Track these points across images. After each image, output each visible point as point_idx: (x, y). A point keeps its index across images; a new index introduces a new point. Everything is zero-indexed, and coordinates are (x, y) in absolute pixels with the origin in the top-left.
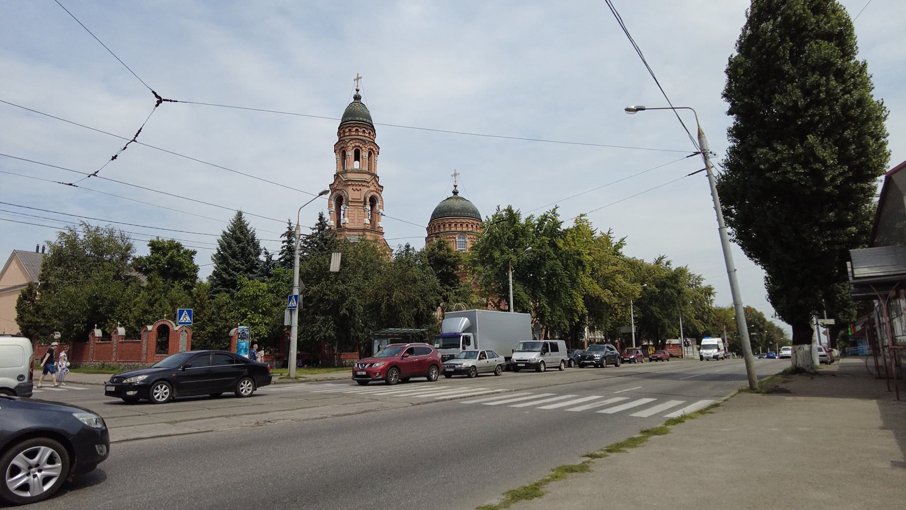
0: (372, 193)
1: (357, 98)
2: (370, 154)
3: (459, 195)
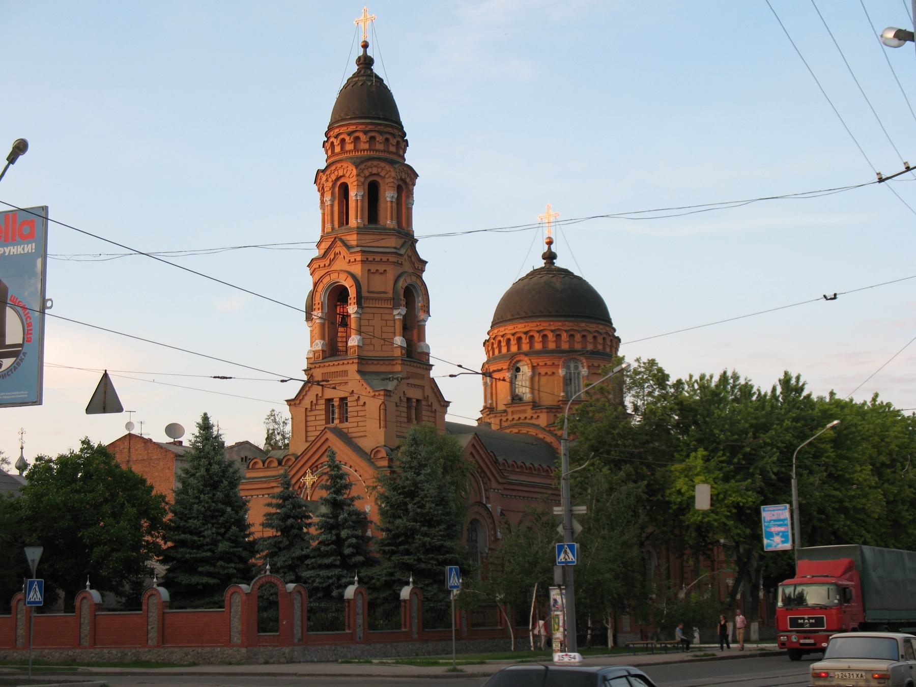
1: (366, 62)
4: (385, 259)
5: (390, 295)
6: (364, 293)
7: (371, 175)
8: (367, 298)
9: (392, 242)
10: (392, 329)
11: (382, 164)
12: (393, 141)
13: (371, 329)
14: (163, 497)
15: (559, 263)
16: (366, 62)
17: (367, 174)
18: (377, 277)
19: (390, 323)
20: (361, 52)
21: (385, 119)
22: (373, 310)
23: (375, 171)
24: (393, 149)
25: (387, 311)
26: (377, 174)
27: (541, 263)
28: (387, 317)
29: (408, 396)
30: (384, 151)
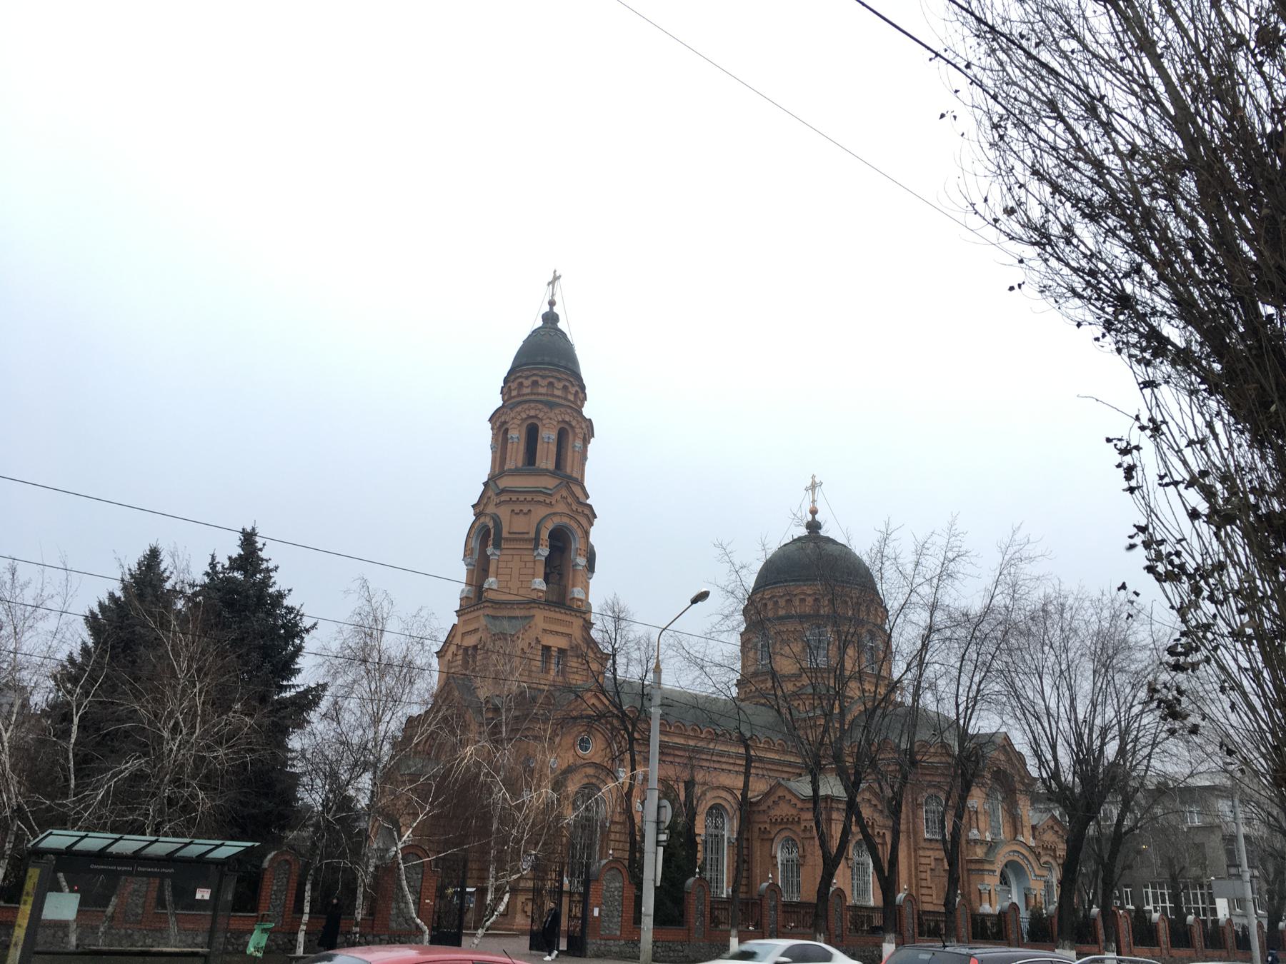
1: (550, 319)
4: (529, 498)
5: (532, 535)
6: (505, 534)
7: (564, 421)
8: (507, 540)
9: (550, 482)
10: (531, 571)
11: (540, 406)
12: (573, 390)
13: (508, 571)
14: (310, 808)
15: (823, 532)
16: (550, 319)
17: (524, 416)
18: (522, 518)
19: (530, 565)
20: (547, 308)
21: (549, 364)
23: (532, 413)
24: (571, 397)
26: (536, 417)
27: (803, 532)
28: (527, 558)
29: (544, 643)
30: (532, 394)
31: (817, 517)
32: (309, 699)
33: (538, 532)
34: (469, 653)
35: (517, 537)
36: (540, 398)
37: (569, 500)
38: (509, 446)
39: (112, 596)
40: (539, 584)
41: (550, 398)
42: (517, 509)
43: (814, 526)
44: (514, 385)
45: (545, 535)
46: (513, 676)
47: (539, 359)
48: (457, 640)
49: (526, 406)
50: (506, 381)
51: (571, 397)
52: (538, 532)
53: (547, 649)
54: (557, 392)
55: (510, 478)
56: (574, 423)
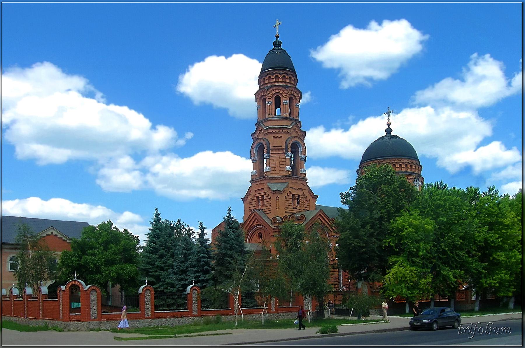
0: (293, 140)
1: (277, 44)
2: (291, 99)
3: (392, 133)
6: (271, 148)
7: (276, 93)
8: (272, 150)
11: (281, 88)
12: (293, 79)
16: (277, 44)
17: (274, 92)
22: (276, 155)
25: (282, 155)
27: (385, 134)
28: (282, 157)
30: (276, 82)
31: (391, 127)
32: (206, 234)
33: (286, 146)
34: (260, 199)
35: (277, 149)
36: (272, 84)
37: (297, 130)
38: (268, 107)
39: (150, 229)
40: (288, 168)
41: (285, 84)
42: (276, 136)
43: (389, 131)
44: (262, 80)
45: (289, 147)
46: (277, 209)
47: (278, 66)
48: (253, 194)
49: (274, 88)
50: (260, 77)
51: (293, 82)
52: (286, 146)
53: (293, 195)
54: (281, 80)
55: (270, 122)
56: (295, 95)
